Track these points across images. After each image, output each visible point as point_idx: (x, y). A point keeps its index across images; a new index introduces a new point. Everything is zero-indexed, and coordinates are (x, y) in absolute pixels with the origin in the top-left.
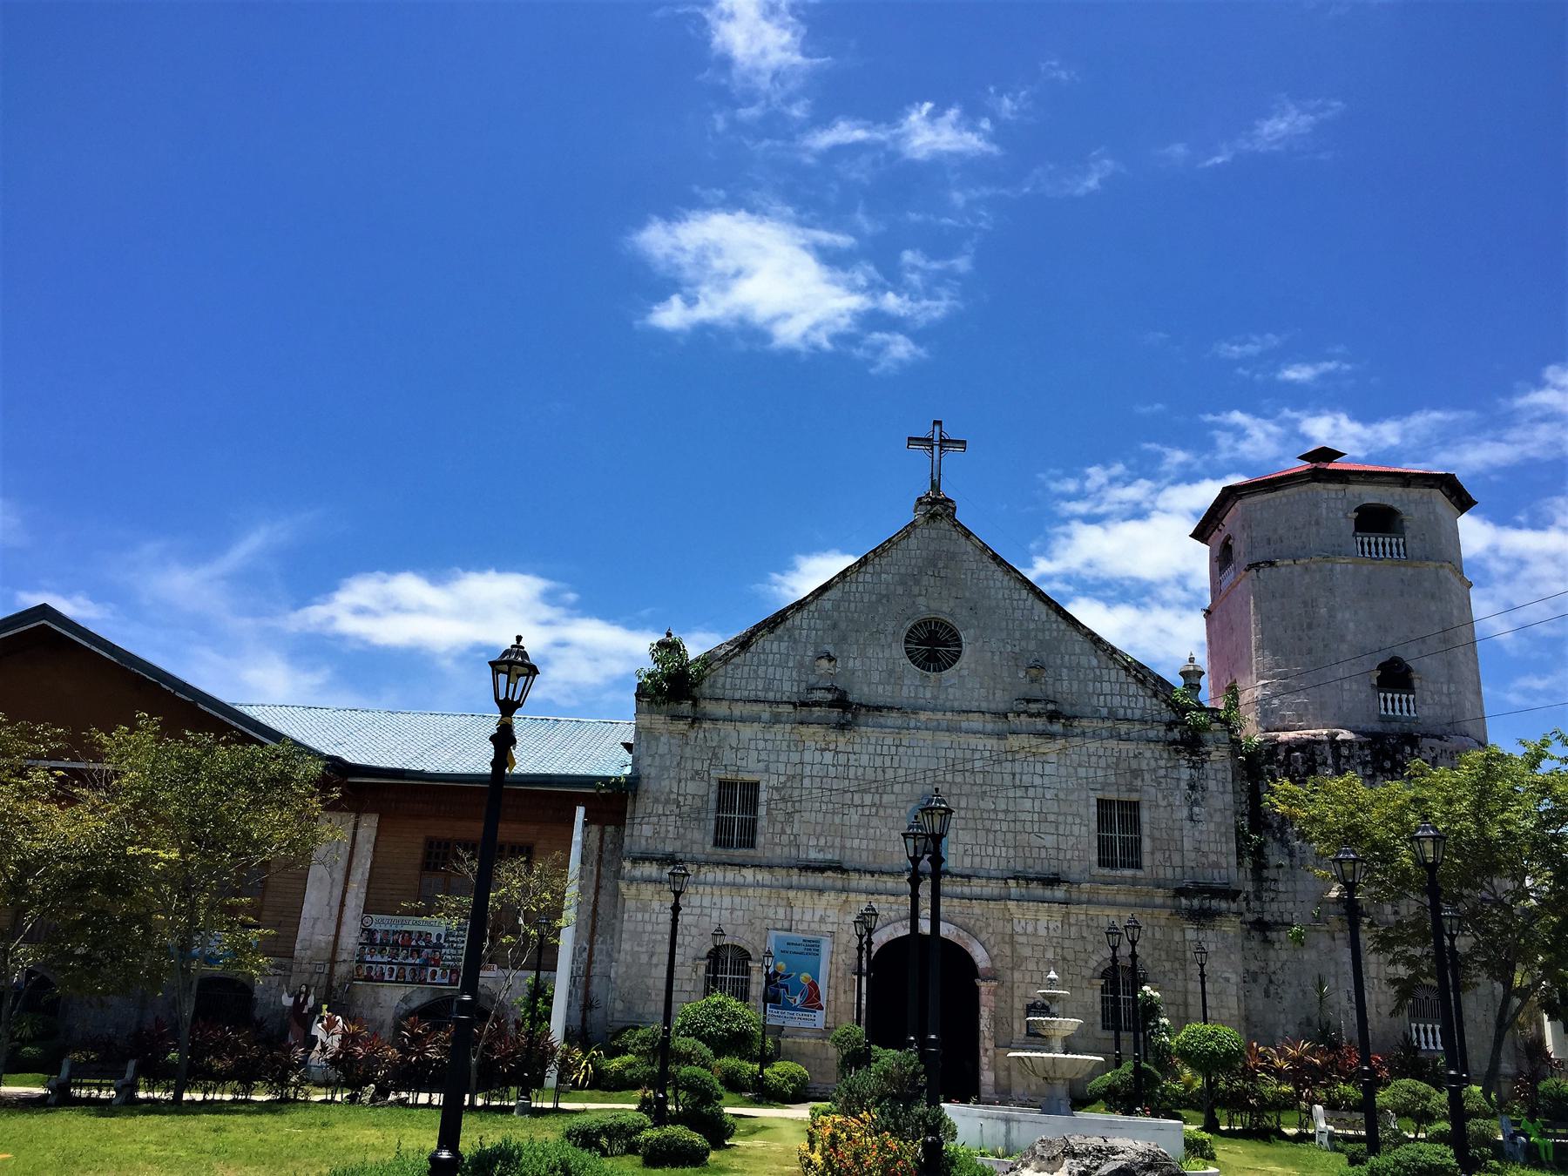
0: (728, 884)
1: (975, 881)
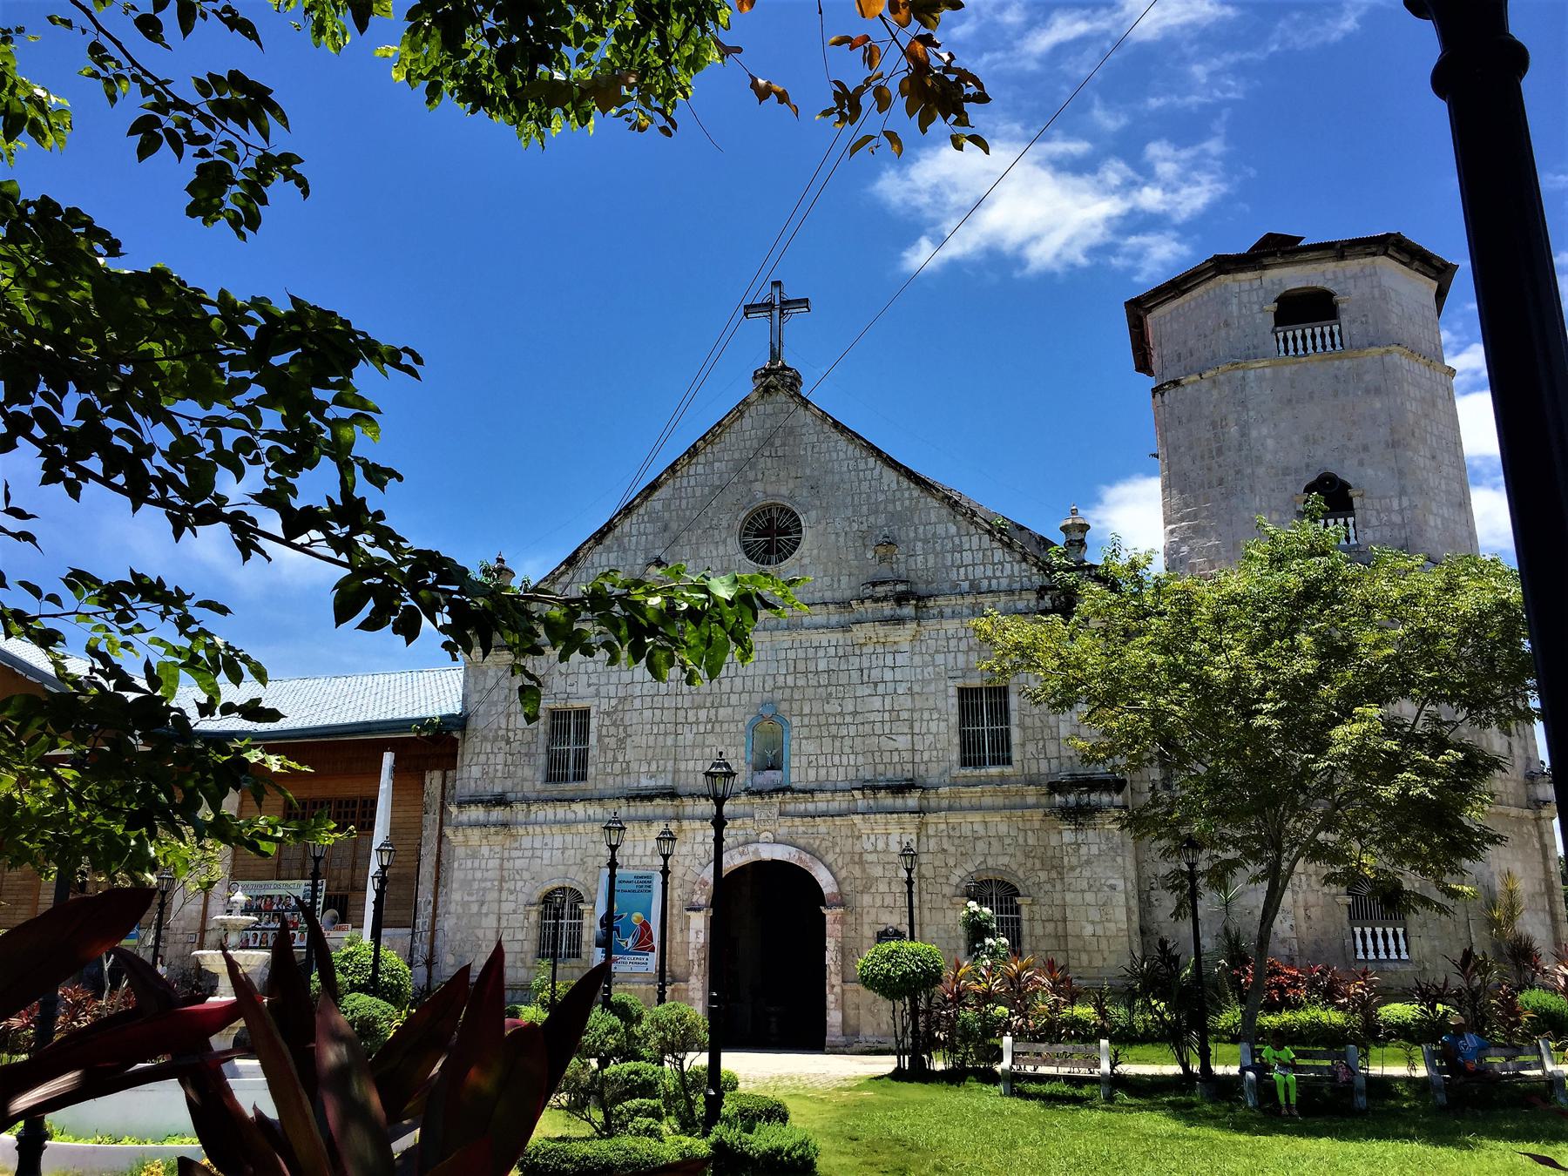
0: (559, 822)
1: (818, 796)
